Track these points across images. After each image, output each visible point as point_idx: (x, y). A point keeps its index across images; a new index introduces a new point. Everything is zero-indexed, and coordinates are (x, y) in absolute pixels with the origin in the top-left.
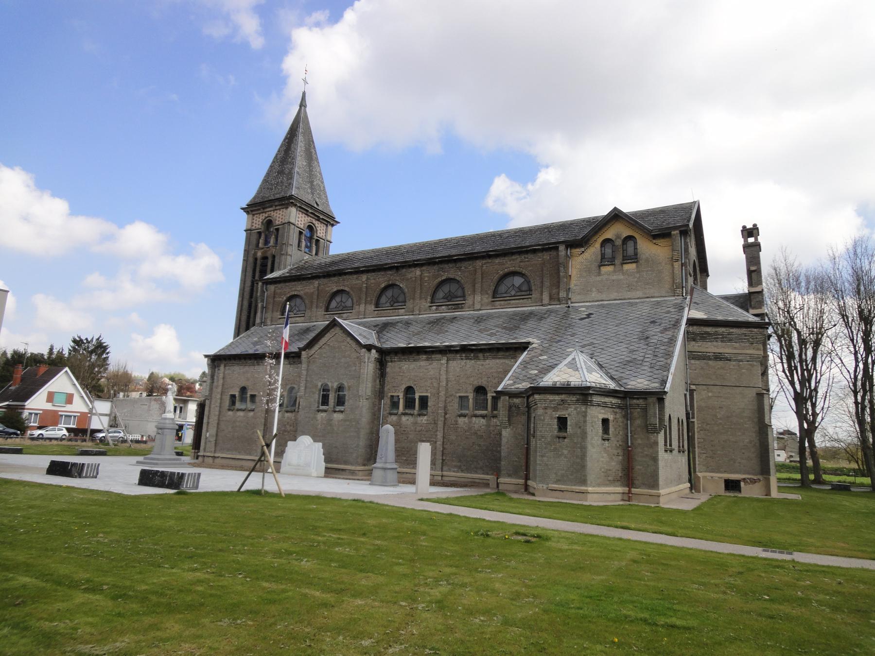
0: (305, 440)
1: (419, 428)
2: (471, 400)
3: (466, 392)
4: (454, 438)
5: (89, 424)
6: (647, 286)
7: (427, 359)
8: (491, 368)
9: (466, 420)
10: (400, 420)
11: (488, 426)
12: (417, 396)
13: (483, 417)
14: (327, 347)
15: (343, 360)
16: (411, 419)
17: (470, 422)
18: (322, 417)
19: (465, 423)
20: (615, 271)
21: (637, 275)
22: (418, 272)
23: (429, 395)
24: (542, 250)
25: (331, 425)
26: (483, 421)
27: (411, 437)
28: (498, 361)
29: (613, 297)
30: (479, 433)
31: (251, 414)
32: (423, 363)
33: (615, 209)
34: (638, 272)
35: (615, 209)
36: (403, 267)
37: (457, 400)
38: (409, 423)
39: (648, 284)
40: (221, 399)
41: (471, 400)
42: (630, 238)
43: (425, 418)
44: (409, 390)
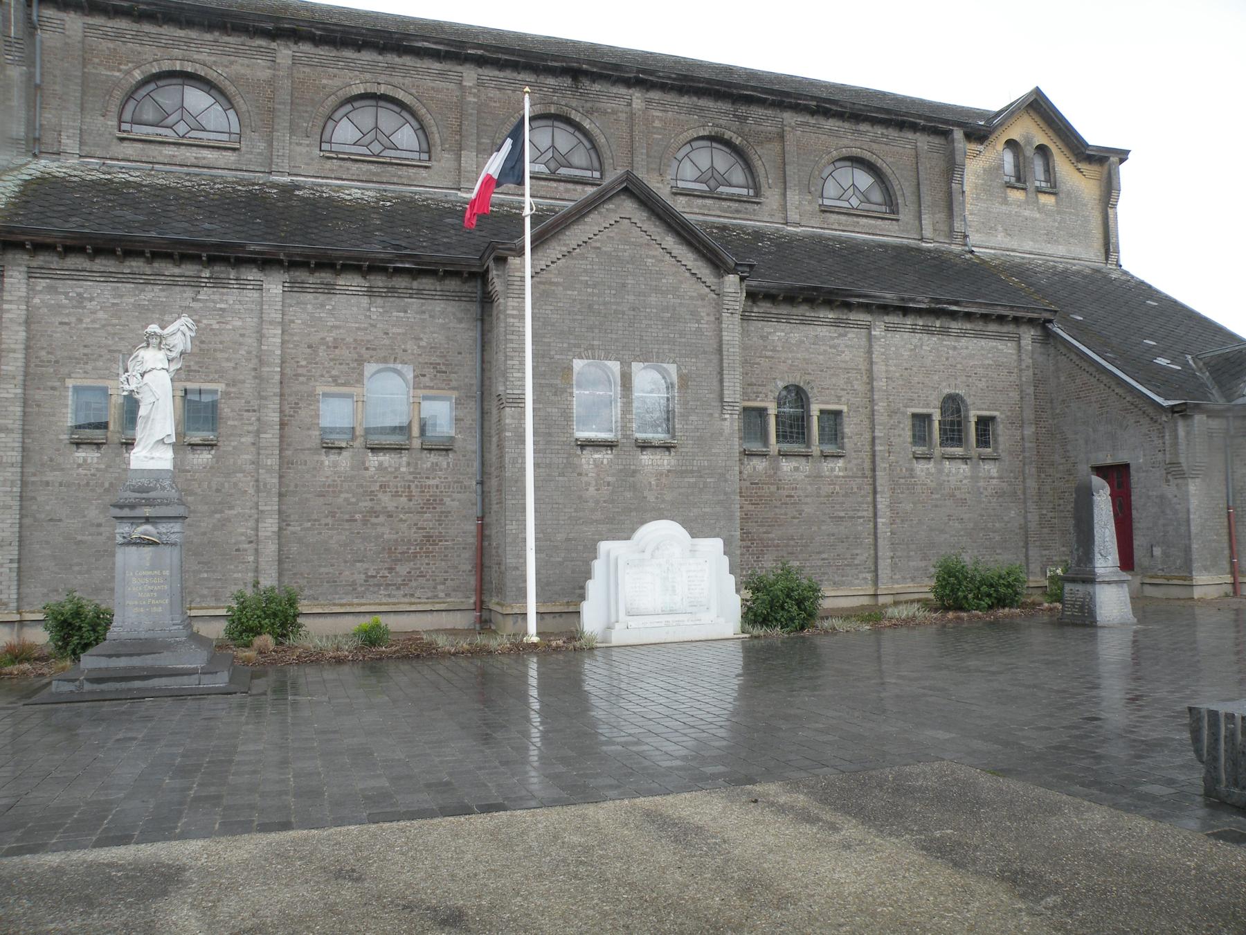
0: (663, 533)
1: (826, 489)
2: (936, 425)
3: (928, 406)
4: (909, 507)
5: (168, 470)
6: (1072, 240)
7: (836, 323)
8: (972, 356)
9: (931, 466)
10: (777, 468)
11: (975, 478)
12: (815, 409)
13: (965, 459)
14: (592, 255)
15: (653, 299)
16: (805, 466)
17: (940, 471)
18: (598, 464)
19: (929, 474)
20: (1027, 202)
21: (1058, 218)
22: (637, 98)
23: (845, 408)
24: (924, 130)
25: (633, 487)
26: (964, 468)
27: (808, 510)
28: (983, 342)
29: (1028, 248)
30: (957, 493)
31: (205, 457)
32: (823, 331)
33: (1037, 91)
34: (1059, 212)
35: (1037, 91)
36: (595, 77)
37: (908, 423)
38: (799, 476)
39: (1072, 236)
40: (871, 363)
41: (936, 425)
42: (1042, 150)
43: (840, 463)
44: (798, 395)
